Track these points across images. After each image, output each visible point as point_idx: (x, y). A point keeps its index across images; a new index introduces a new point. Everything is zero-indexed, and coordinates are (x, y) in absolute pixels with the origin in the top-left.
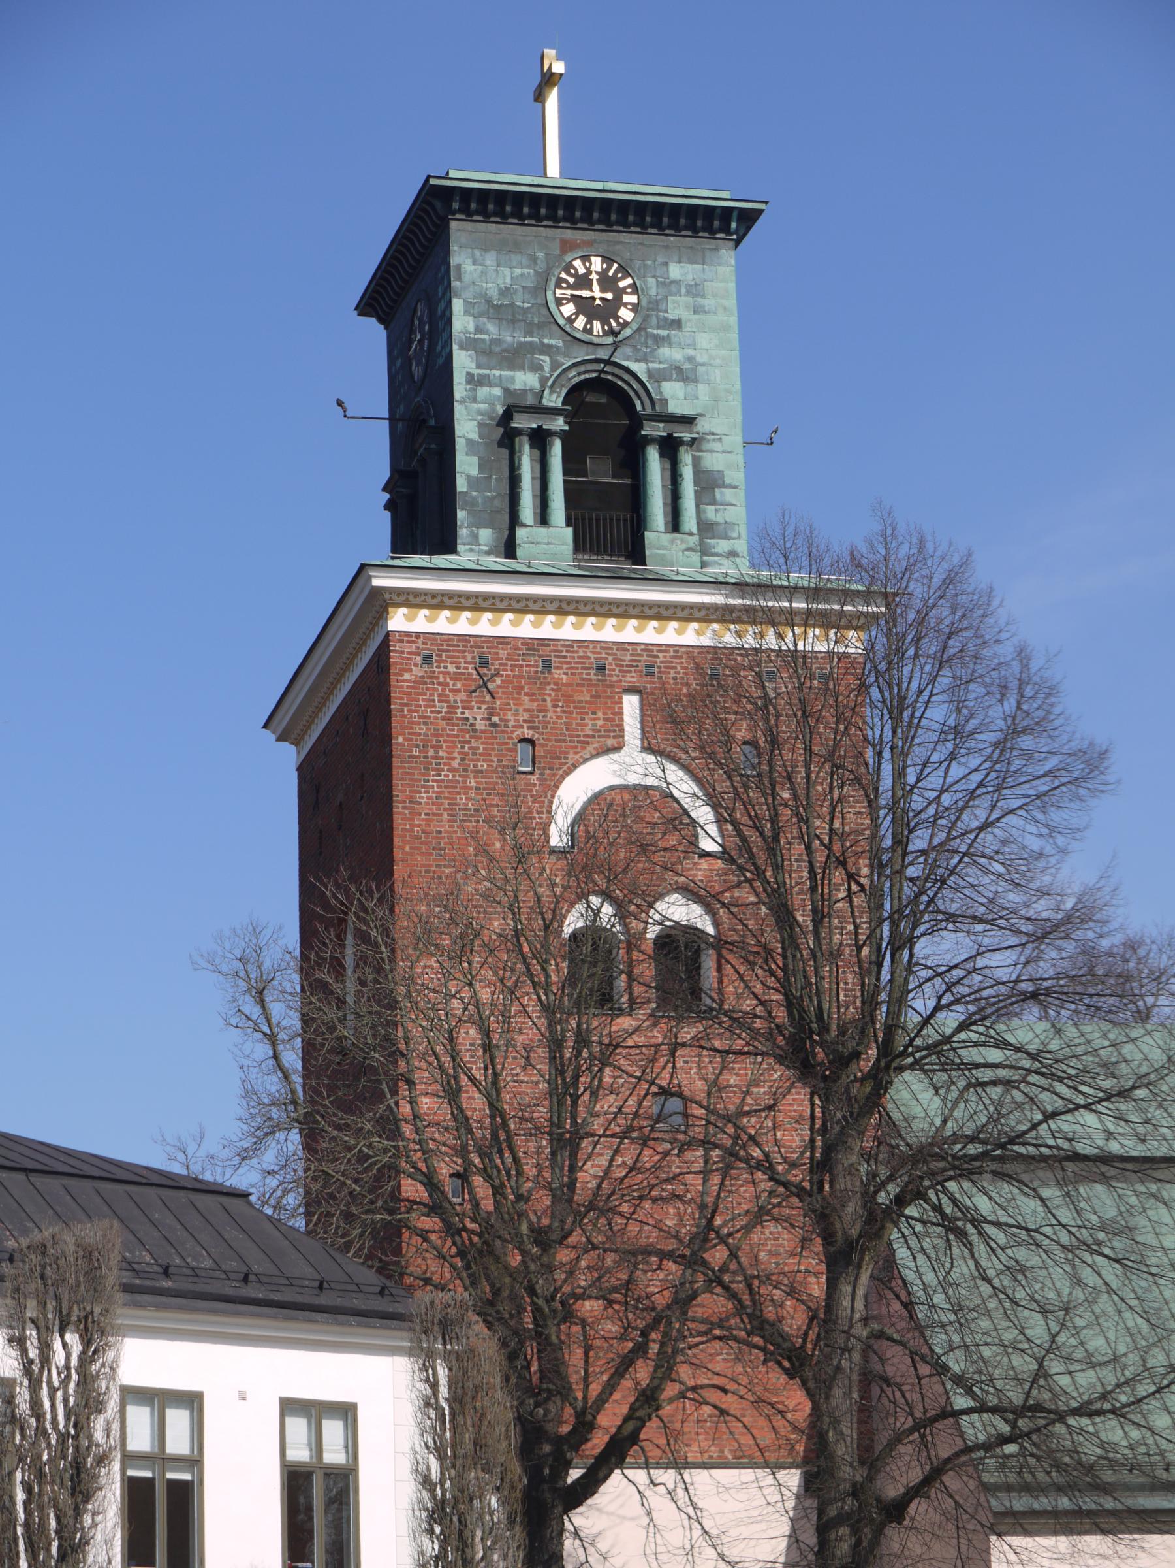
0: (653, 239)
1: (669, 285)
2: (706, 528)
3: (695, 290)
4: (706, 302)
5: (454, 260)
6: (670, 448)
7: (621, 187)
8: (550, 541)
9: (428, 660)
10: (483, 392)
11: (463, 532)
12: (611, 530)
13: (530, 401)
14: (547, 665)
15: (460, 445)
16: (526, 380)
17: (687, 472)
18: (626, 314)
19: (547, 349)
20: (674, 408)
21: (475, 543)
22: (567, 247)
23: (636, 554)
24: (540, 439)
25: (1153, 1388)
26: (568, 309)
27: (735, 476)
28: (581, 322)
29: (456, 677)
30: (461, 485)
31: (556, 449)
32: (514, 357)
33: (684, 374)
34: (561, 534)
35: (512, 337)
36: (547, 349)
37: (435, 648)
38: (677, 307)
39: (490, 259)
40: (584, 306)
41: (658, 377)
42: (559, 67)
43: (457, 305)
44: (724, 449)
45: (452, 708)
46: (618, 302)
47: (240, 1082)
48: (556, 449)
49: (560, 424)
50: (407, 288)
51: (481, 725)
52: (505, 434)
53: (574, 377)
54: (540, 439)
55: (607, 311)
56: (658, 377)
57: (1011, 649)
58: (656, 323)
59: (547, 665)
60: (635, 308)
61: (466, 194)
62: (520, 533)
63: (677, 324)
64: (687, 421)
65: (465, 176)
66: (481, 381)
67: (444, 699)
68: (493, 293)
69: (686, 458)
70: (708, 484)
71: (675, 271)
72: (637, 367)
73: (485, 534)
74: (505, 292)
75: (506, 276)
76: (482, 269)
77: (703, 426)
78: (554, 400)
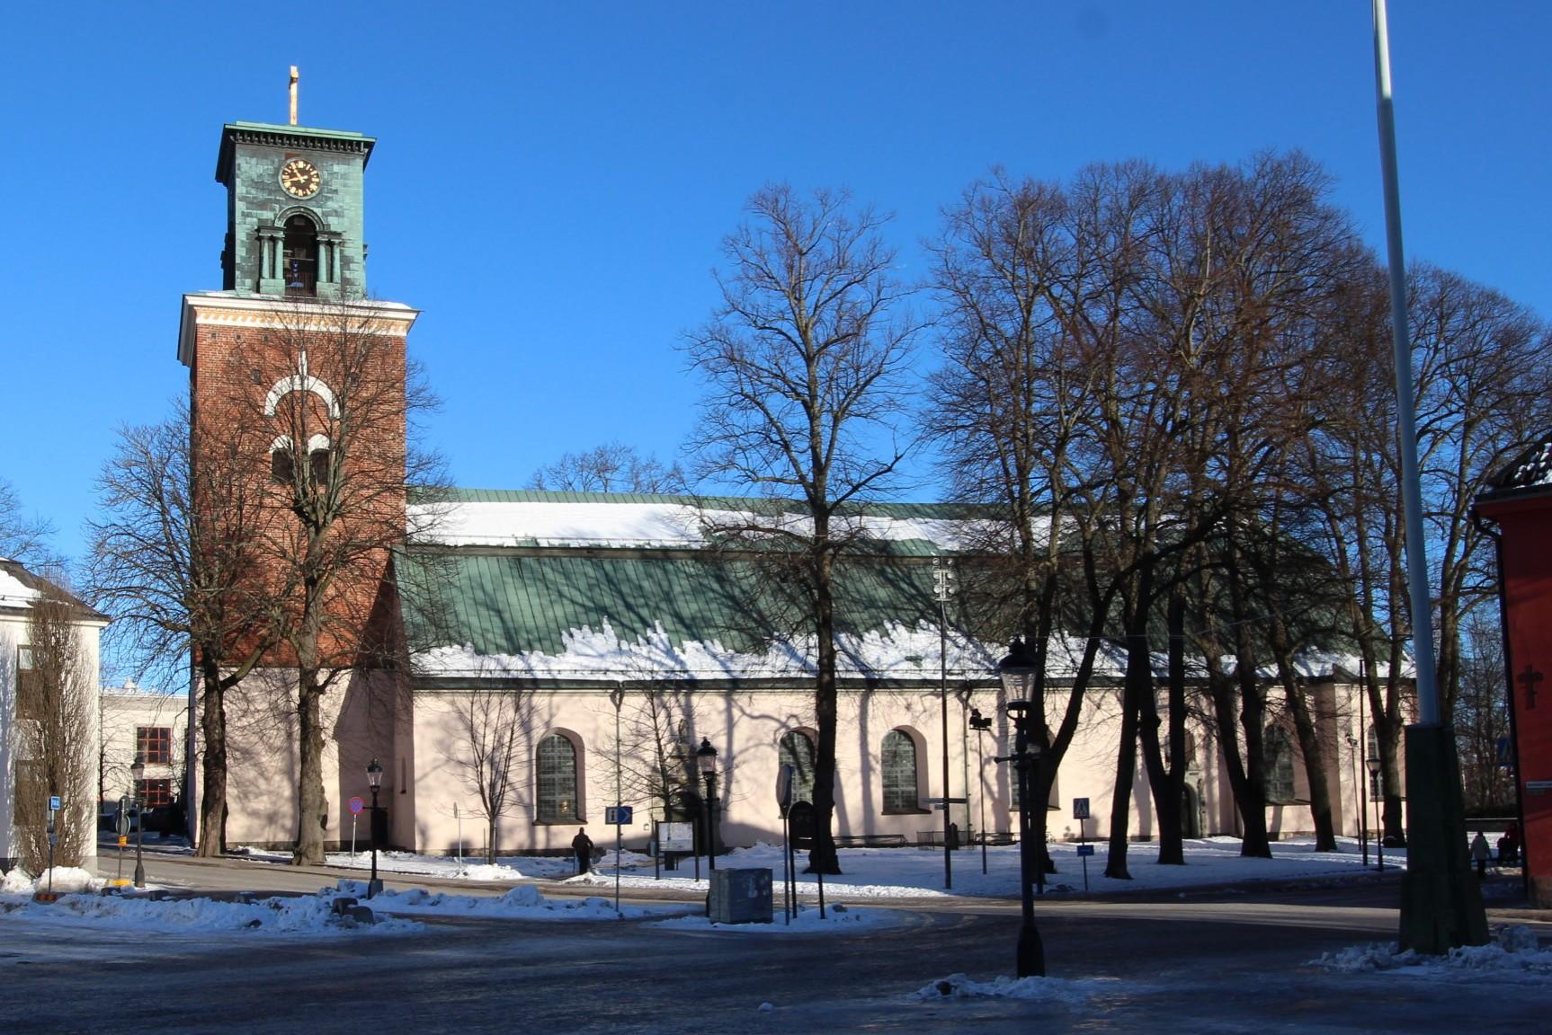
0: (327, 154)
1: (332, 174)
2: (346, 281)
3: (344, 176)
6: (330, 244)
7: (313, 131)
11: (238, 281)
12: (303, 280)
15: (238, 242)
16: (267, 215)
17: (337, 256)
18: (313, 187)
19: (277, 202)
20: (333, 229)
21: (243, 283)
22: (288, 156)
23: (312, 289)
25: (540, 700)
26: (293, 190)
30: (238, 260)
32: (263, 205)
33: (336, 213)
34: (280, 281)
35: (262, 196)
36: (277, 202)
37: (215, 332)
39: (254, 161)
41: (326, 215)
43: (238, 181)
44: (354, 249)
46: (309, 181)
47: (629, 446)
48: (280, 245)
49: (281, 235)
52: (257, 238)
54: (273, 240)
56: (326, 215)
57: (770, 658)
58: (325, 192)
61: (242, 132)
64: (338, 235)
65: (242, 125)
66: (249, 215)
69: (337, 250)
70: (346, 262)
71: (336, 168)
72: (318, 211)
73: (248, 282)
74: (260, 176)
75: (260, 169)
76: (249, 166)
77: (345, 236)
78: (280, 224)
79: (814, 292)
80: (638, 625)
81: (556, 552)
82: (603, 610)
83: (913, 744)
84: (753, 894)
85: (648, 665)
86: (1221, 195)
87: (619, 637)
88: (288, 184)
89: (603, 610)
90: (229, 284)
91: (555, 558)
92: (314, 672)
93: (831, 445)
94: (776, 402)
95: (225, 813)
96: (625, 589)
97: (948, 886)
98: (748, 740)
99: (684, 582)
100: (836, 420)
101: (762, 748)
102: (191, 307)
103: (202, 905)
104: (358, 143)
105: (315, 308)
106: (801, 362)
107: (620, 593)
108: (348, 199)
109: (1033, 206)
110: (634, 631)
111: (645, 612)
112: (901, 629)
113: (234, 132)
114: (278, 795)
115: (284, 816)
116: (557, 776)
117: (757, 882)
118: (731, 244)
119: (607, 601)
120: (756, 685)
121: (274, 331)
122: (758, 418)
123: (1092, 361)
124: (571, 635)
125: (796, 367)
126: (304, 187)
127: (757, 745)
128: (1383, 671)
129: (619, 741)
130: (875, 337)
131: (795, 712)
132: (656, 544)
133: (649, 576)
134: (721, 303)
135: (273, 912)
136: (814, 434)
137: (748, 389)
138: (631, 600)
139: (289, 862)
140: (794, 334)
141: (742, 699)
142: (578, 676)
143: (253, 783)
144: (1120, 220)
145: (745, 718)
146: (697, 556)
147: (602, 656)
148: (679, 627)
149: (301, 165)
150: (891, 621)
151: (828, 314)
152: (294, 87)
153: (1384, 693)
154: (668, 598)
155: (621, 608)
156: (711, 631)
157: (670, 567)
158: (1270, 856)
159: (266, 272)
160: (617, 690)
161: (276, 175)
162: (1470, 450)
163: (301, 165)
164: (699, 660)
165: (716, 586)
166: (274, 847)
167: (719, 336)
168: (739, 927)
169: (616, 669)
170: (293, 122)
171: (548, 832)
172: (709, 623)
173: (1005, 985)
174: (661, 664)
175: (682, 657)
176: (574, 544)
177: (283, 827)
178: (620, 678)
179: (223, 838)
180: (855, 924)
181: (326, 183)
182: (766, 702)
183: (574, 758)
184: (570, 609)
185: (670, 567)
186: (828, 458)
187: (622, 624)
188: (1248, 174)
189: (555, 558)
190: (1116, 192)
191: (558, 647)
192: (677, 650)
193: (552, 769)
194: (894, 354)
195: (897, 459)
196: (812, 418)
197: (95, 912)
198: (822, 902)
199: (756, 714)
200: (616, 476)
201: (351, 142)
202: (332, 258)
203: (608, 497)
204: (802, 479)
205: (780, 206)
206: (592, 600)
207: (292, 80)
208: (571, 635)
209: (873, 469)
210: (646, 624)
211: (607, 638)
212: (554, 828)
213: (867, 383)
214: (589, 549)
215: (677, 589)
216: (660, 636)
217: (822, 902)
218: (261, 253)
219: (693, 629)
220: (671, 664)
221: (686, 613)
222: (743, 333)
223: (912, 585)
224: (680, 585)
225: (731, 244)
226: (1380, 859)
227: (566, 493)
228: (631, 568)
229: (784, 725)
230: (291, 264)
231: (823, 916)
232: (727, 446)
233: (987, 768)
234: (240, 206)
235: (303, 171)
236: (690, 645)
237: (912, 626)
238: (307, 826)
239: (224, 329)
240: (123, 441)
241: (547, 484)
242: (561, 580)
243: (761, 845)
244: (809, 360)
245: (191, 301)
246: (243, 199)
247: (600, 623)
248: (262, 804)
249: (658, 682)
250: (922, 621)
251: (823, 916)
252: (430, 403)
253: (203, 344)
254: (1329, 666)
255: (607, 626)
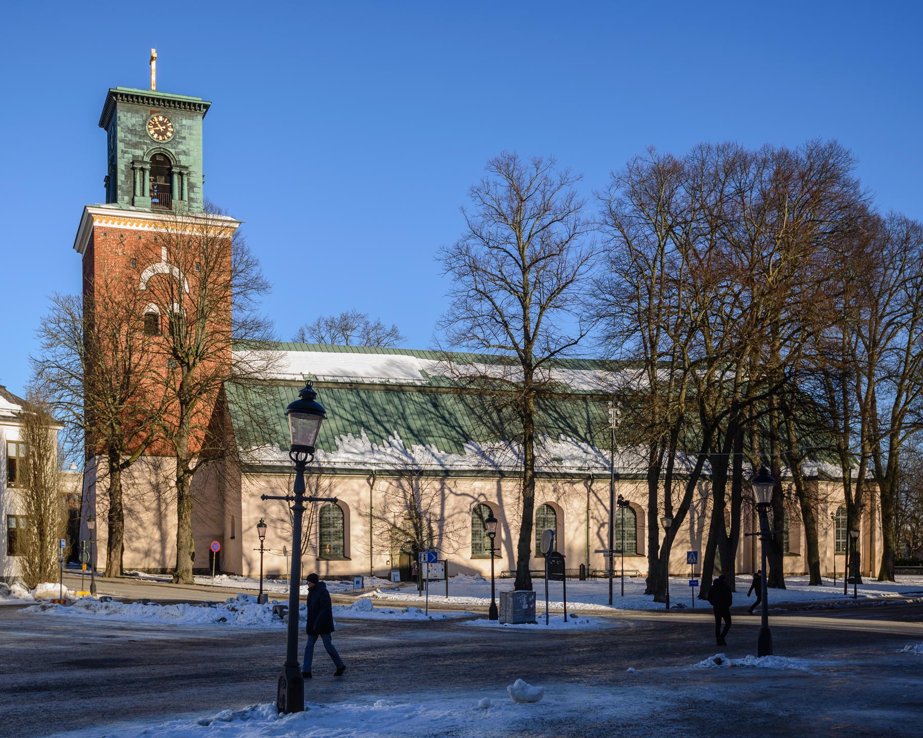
0: (178, 112)
3: (190, 128)
4: (194, 132)
5: (118, 115)
6: (181, 174)
7: (169, 96)
8: (146, 201)
9: (105, 234)
10: (126, 155)
11: (119, 197)
12: (163, 198)
13: (140, 159)
14: (140, 238)
15: (119, 171)
16: (139, 153)
17: (185, 183)
18: (169, 134)
19: (145, 144)
20: (182, 164)
21: (123, 199)
22: (152, 112)
24: (142, 169)
27: (200, 184)
28: (156, 136)
29: (113, 240)
30: (119, 183)
31: (147, 173)
32: (136, 146)
33: (185, 153)
34: (147, 200)
35: (135, 139)
36: (145, 144)
37: (106, 232)
38: (184, 133)
39: (129, 115)
40: (158, 132)
41: (178, 154)
42: (155, 55)
43: (119, 129)
45: (112, 249)
46: (166, 130)
47: (363, 314)
48: (147, 173)
49: (148, 166)
50: (108, 120)
51: (120, 254)
53: (153, 152)
55: (163, 134)
56: (178, 154)
58: (178, 138)
59: (140, 238)
60: (172, 132)
61: (122, 95)
62: (136, 198)
63: (184, 138)
64: (186, 168)
65: (121, 89)
66: (126, 152)
67: (110, 246)
68: (130, 126)
69: (185, 178)
70: (191, 187)
71: (184, 122)
72: (173, 151)
73: (126, 198)
74: (133, 125)
75: (134, 121)
76: (126, 118)
77: (191, 169)
78: (147, 159)
79: (529, 226)
80: (384, 434)
81: (330, 385)
82: (361, 424)
83: (555, 514)
84: (525, 606)
85: (394, 461)
86: (783, 167)
87: (372, 442)
88: (152, 132)
89: (361, 424)
90: (112, 198)
91: (328, 388)
92: (187, 461)
93: (537, 326)
94: (501, 297)
95: (123, 549)
96: (375, 410)
97: (610, 603)
98: (454, 509)
99: (412, 407)
100: (543, 308)
101: (463, 514)
102: (90, 215)
103: (184, 608)
104: (200, 105)
105: (172, 218)
106: (518, 270)
107: (372, 412)
108: (192, 144)
109: (666, 173)
110: (382, 438)
111: (388, 426)
112: (549, 440)
113: (116, 94)
114: (152, 539)
115: (155, 552)
116: (332, 530)
117: (527, 600)
118: (475, 192)
119: (364, 418)
120: (461, 474)
121: (160, 234)
122: (486, 306)
123: (704, 278)
124: (341, 440)
125: (517, 278)
126: (163, 134)
127: (459, 513)
128: (855, 474)
129: (372, 508)
130: (571, 257)
131: (483, 492)
132: (392, 381)
133: (390, 402)
134: (467, 231)
135: (232, 613)
136: (526, 318)
137: (481, 287)
138: (378, 417)
139: (171, 582)
140: (515, 253)
141: (449, 483)
142: (347, 466)
143: (136, 531)
144: (717, 183)
145: (452, 495)
146: (421, 390)
147: (362, 454)
148: (410, 436)
149: (161, 119)
150: (543, 435)
151: (536, 241)
152: (154, 63)
153: (854, 487)
154: (404, 417)
155: (373, 423)
156: (430, 439)
157: (403, 397)
158: (785, 588)
159: (138, 192)
160: (372, 476)
161: (144, 125)
162: (914, 336)
163: (161, 119)
164: (422, 456)
165: (433, 410)
166: (149, 571)
167: (461, 251)
168: (520, 626)
169: (372, 461)
170: (154, 88)
171: (327, 565)
172: (429, 433)
173: (750, 660)
174: (398, 458)
175: (413, 455)
176: (340, 380)
177: (155, 559)
178: (373, 468)
179: (121, 566)
180: (587, 625)
181: (178, 132)
182: (464, 485)
183: (343, 519)
184: (339, 423)
185: (403, 397)
186: (534, 335)
187: (374, 433)
188: (803, 156)
189: (328, 388)
190: (715, 162)
191: (334, 447)
192: (409, 451)
193: (329, 525)
194: (583, 269)
195: (582, 336)
196: (525, 308)
197: (104, 612)
198: (565, 613)
199: (459, 492)
200: (355, 333)
201: (194, 104)
202: (182, 184)
203: (348, 349)
204: (516, 346)
205: (511, 168)
206: (353, 416)
207: (152, 58)
208: (341, 440)
209: (563, 342)
210: (389, 433)
211: (363, 443)
212: (331, 563)
213: (564, 287)
214: (351, 384)
215: (408, 412)
216: (397, 441)
217: (565, 613)
218: (134, 179)
219: (419, 437)
220: (405, 458)
221: (413, 427)
222: (479, 250)
223: (556, 411)
224: (410, 409)
225: (475, 192)
226: (855, 591)
227: (322, 345)
228: (379, 397)
229: (476, 500)
230: (153, 186)
231: (566, 621)
232: (469, 323)
233: (602, 529)
234: (120, 146)
235: (162, 123)
236: (418, 448)
237: (557, 439)
238: (182, 559)
239: (112, 230)
240: (54, 305)
241: (307, 336)
242: (333, 403)
243: (461, 575)
244: (525, 270)
245: (91, 210)
246: (122, 141)
247: (359, 432)
248: (142, 544)
249: (398, 471)
250: (562, 437)
251: (566, 621)
252: (262, 287)
253: (98, 240)
254: (815, 469)
255: (364, 435)
